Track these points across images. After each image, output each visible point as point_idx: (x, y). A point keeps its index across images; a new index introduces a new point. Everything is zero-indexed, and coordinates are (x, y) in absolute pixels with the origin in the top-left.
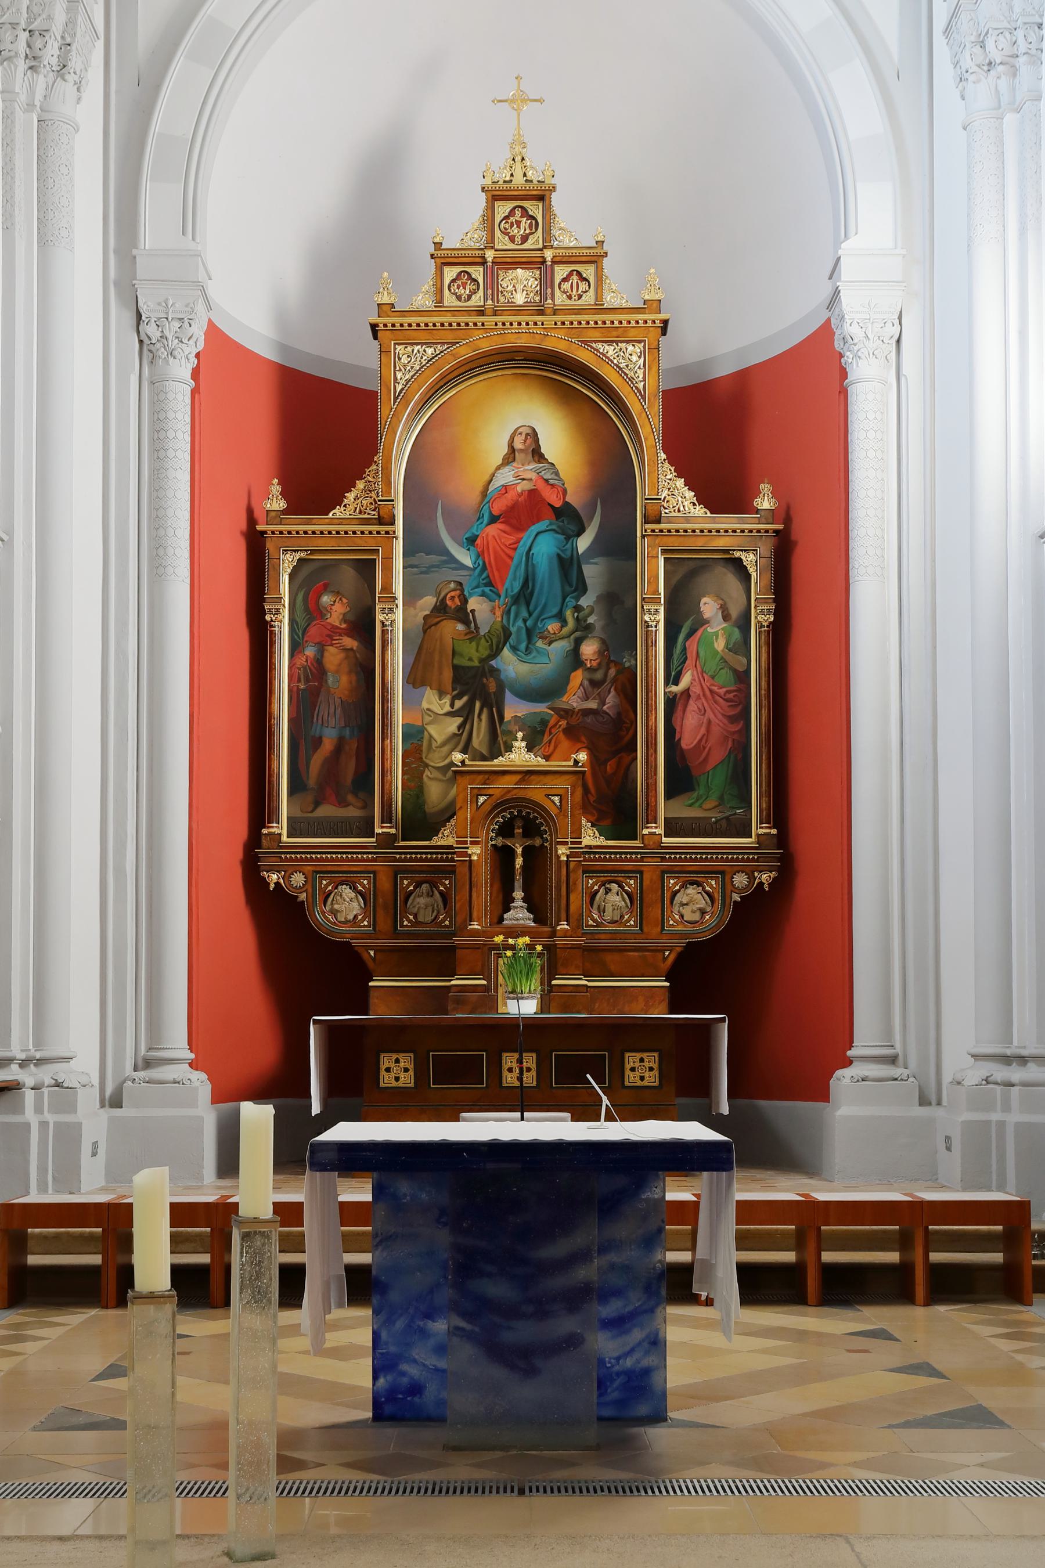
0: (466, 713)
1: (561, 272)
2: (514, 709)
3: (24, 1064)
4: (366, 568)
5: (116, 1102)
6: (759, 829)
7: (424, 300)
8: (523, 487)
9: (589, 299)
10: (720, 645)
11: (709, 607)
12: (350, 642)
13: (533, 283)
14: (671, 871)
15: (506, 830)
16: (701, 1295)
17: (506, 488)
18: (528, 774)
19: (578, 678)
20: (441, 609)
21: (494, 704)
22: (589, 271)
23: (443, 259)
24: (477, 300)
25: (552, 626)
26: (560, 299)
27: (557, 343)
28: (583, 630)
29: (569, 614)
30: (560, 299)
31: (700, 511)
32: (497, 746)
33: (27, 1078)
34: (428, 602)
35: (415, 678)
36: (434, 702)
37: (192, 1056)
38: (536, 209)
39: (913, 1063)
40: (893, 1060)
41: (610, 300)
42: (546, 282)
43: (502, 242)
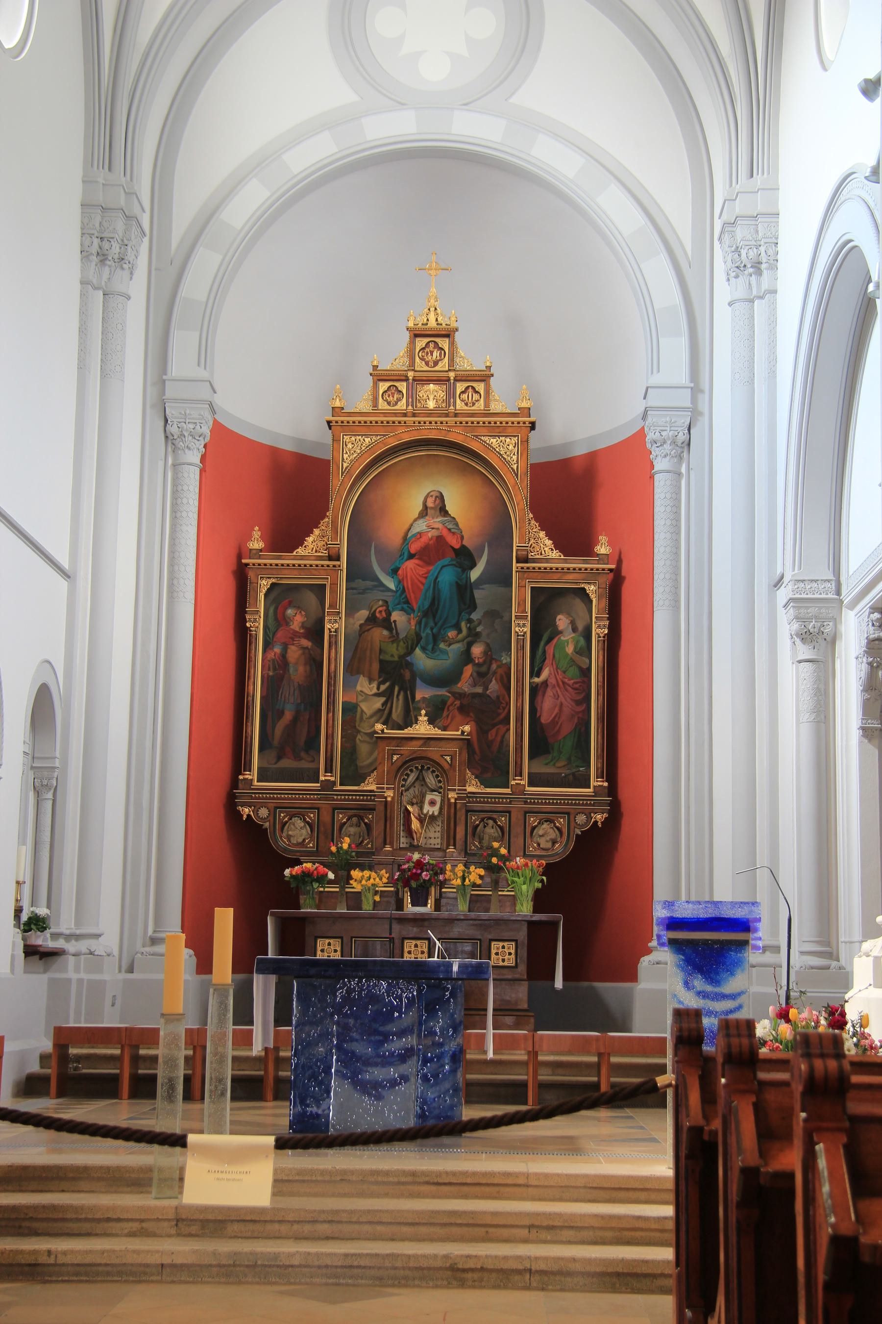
0: (388, 695)
1: (460, 387)
2: (423, 692)
3: (69, 937)
5: (131, 970)
7: (365, 406)
8: (432, 534)
9: (480, 405)
10: (570, 649)
11: (562, 622)
12: (306, 643)
13: (442, 394)
17: (420, 534)
18: (428, 740)
19: (468, 670)
20: (372, 620)
21: (409, 689)
23: (379, 376)
24: (402, 405)
25: (451, 634)
28: (474, 636)
30: (460, 405)
31: (555, 554)
32: (409, 720)
35: (353, 668)
36: (365, 686)
38: (444, 343)
42: (451, 394)
43: (419, 365)
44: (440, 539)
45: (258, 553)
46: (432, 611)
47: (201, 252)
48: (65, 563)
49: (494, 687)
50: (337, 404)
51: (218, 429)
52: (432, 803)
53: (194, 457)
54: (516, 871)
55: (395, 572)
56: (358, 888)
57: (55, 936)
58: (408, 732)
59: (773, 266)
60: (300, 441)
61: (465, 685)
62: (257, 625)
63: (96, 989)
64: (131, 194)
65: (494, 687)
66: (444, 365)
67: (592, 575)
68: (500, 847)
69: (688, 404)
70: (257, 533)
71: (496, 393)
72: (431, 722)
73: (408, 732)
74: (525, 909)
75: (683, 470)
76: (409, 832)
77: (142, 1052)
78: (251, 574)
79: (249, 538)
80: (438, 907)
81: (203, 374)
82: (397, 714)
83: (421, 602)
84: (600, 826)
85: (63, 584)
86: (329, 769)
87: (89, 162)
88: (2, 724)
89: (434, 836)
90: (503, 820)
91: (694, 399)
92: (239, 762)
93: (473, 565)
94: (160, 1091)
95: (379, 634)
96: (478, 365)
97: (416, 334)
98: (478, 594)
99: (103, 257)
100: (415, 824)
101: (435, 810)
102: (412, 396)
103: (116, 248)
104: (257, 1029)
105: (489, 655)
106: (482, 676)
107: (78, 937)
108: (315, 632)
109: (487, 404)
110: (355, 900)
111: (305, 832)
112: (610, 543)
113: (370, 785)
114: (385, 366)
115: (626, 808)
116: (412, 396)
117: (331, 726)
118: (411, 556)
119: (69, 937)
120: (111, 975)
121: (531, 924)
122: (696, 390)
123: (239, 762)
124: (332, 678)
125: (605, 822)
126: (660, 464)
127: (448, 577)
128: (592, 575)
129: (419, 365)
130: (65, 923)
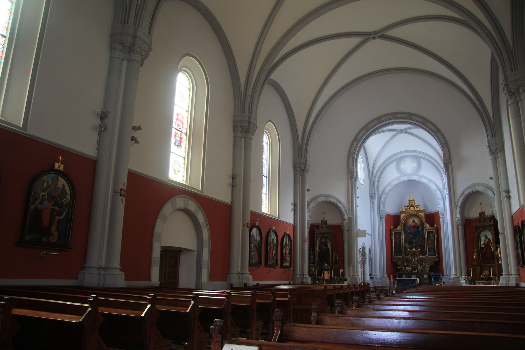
1: (416, 207)
2: (414, 245)
3: (374, 276)
5: (381, 279)
6: (437, 255)
7: (404, 210)
8: (414, 225)
9: (418, 209)
10: (432, 239)
11: (431, 235)
12: (399, 239)
13: (414, 208)
14: (429, 259)
17: (412, 225)
18: (415, 251)
19: (420, 242)
20: (407, 236)
22: (418, 207)
23: (405, 207)
24: (408, 210)
25: (417, 237)
27: (416, 213)
28: (420, 237)
29: (419, 236)
31: (429, 227)
32: (413, 249)
33: (374, 277)
34: (406, 235)
36: (407, 244)
37: (121, 267)
38: (413, 202)
39: (449, 276)
40: (447, 276)
41: (420, 209)
42: (415, 208)
43: (410, 205)
44: (415, 226)
45: (392, 229)
47: (383, 195)
48: (370, 234)
49: (423, 244)
50: (401, 210)
51: (386, 214)
52: (416, 259)
53: (384, 219)
54: (426, 267)
55: (409, 230)
56: (407, 269)
57: (373, 276)
60: (396, 214)
61: (419, 243)
63: (378, 282)
64: (375, 191)
65: (423, 244)
67: (434, 229)
69: (443, 209)
70: (392, 227)
71: (420, 208)
72: (415, 249)
74: (428, 271)
75: (444, 217)
76: (413, 262)
77: (384, 288)
78: (392, 231)
79: (391, 227)
80: (417, 271)
81: (384, 210)
85: (370, 236)
86: (403, 255)
87: (370, 188)
88: (357, 1)
89: (416, 263)
90: (425, 260)
91: (444, 208)
92: (392, 254)
93: (419, 228)
98: (420, 232)
99: (372, 198)
100: (414, 261)
101: (416, 259)
102: (410, 208)
103: (373, 197)
104: (395, 286)
107: (375, 276)
108: (400, 238)
109: (419, 209)
110: (407, 271)
111: (401, 263)
112: (436, 225)
116: (410, 208)
117: (403, 249)
118: (411, 228)
119: (374, 276)
120: (379, 280)
124: (403, 243)
125: (438, 260)
126: (441, 217)
127: (416, 230)
128: (434, 229)
130: (374, 274)
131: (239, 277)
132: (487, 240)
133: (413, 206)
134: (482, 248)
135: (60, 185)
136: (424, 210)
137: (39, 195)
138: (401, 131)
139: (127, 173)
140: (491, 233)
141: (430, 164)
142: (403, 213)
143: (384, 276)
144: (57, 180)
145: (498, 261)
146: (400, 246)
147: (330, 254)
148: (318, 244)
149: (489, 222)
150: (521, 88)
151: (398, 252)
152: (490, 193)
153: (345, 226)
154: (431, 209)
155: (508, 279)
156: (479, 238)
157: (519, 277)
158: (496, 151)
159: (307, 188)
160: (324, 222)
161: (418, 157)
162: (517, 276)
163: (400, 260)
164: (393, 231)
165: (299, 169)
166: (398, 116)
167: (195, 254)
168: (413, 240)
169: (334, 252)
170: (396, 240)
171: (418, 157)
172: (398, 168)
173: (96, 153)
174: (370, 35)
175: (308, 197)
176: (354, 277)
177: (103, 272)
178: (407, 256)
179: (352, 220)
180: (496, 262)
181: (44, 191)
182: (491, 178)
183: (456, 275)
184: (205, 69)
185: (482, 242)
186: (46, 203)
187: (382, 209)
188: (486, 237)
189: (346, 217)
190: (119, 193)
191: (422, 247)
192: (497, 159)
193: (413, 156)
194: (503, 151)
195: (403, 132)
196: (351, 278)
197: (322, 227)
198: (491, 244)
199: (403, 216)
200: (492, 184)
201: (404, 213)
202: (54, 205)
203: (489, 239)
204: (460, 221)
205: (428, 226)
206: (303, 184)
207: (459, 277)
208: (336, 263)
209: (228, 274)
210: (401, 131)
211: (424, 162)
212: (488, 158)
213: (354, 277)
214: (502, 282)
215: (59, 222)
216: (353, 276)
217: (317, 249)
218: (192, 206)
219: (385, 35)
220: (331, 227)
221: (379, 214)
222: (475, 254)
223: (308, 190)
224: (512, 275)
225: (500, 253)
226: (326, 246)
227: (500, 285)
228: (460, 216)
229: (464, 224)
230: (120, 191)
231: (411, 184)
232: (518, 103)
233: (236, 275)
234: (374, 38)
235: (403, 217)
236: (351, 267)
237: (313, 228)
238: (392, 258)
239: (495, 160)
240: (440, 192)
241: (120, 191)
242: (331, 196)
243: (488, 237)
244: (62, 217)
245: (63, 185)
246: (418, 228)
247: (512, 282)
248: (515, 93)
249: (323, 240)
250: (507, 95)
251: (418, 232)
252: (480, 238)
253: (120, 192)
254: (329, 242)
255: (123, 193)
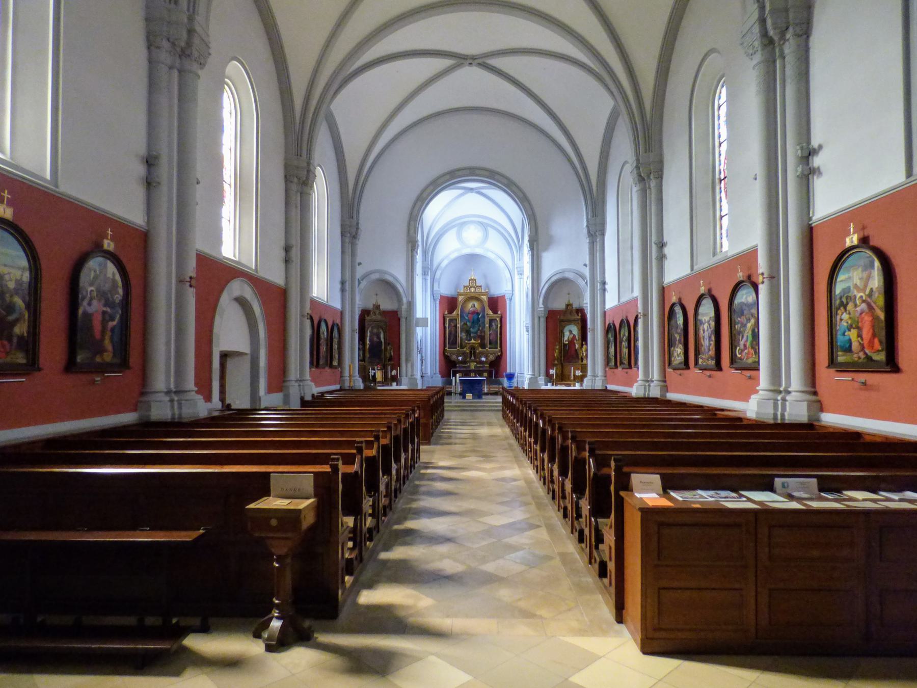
0: (467, 336)
2: (472, 335)
4: (456, 320)
5: (432, 378)
7: (462, 291)
11: (493, 324)
15: (472, 349)
16: (608, 517)
18: (473, 343)
20: (464, 324)
21: (470, 335)
23: (465, 287)
26: (477, 291)
27: (477, 296)
28: (480, 326)
30: (477, 291)
31: (492, 314)
32: (470, 340)
34: (463, 323)
35: (461, 332)
36: (463, 334)
37: (196, 389)
38: (474, 281)
45: (446, 314)
46: (473, 322)
53: (438, 302)
55: (467, 316)
58: (470, 342)
59: (523, 274)
62: (447, 326)
66: (474, 285)
67: (498, 317)
68: (557, 349)
71: (482, 289)
73: (470, 342)
79: (445, 312)
82: (468, 338)
83: (472, 321)
84: (852, 224)
92: (445, 346)
94: (390, 425)
95: (465, 326)
96: (480, 285)
97: (470, 280)
98: (481, 320)
105: (482, 329)
106: (481, 332)
108: (456, 326)
113: (465, 350)
114: (465, 285)
115: (503, 352)
121: (489, 370)
122: (513, 291)
123: (445, 346)
126: (508, 302)
127: (476, 317)
128: (498, 317)
129: (471, 285)
131: (299, 386)
132: (572, 336)
133: (474, 287)
134: (565, 345)
135: (110, 275)
136: (487, 292)
137: (87, 291)
138: (471, 190)
139: (195, 255)
140: (578, 328)
141: (500, 235)
142: (460, 295)
143: (435, 374)
144: (105, 266)
145: (582, 360)
146: (455, 337)
147: (383, 348)
148: (368, 335)
149: (576, 315)
150: (652, 174)
151: (453, 343)
152: (581, 283)
153: (403, 313)
154: (496, 292)
155: (593, 382)
156: (562, 333)
157: (605, 378)
158: (595, 233)
159: (358, 260)
160: (377, 307)
161: (485, 225)
162: (604, 378)
163: (454, 354)
164: (448, 317)
165: (349, 235)
166: (478, 172)
167: (247, 360)
168: (471, 329)
169: (389, 344)
170: (450, 329)
171: (485, 225)
172: (459, 235)
173: (146, 221)
174: (466, 59)
175: (360, 272)
176: (413, 377)
177: (176, 398)
178: (463, 349)
179: (411, 305)
180: (580, 361)
181: (91, 284)
182: (585, 265)
183: (534, 375)
184: (251, 76)
185: (566, 338)
186: (95, 302)
187: (436, 288)
188: (571, 332)
189: (405, 300)
190: (189, 283)
191: (482, 338)
192: (595, 243)
193: (479, 222)
194: (603, 234)
195: (474, 191)
196: (409, 378)
197: (375, 313)
198: (575, 341)
199: (460, 298)
200: (586, 272)
201: (462, 295)
202: (105, 305)
203: (574, 335)
204: (543, 312)
205: (491, 313)
206: (353, 254)
207: (537, 378)
208: (390, 359)
209: (284, 381)
210: (471, 190)
211: (492, 233)
212: (585, 242)
213: (413, 377)
214: (587, 384)
215: (112, 330)
216: (411, 375)
217: (368, 342)
218: (248, 293)
219: (487, 64)
220: (385, 313)
221: (433, 294)
222: (557, 351)
223: (360, 264)
224: (598, 376)
225: (586, 351)
226: (379, 338)
227: (585, 388)
228: (543, 306)
229: (547, 316)
230: (189, 280)
231: (472, 259)
232: (646, 190)
233: (293, 383)
234: (470, 64)
235: (461, 300)
236: (409, 365)
237: (364, 313)
238: (444, 350)
239: (592, 244)
240: (509, 271)
241: (189, 280)
242: (386, 273)
243: (573, 332)
244: (115, 323)
245: (114, 274)
246: (478, 314)
247: (599, 385)
248: (646, 178)
249: (375, 331)
250: (636, 179)
251: (478, 319)
252: (564, 333)
253: (190, 282)
254: (382, 333)
255: (193, 282)
